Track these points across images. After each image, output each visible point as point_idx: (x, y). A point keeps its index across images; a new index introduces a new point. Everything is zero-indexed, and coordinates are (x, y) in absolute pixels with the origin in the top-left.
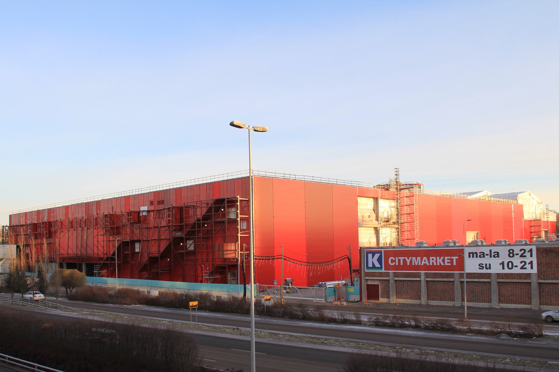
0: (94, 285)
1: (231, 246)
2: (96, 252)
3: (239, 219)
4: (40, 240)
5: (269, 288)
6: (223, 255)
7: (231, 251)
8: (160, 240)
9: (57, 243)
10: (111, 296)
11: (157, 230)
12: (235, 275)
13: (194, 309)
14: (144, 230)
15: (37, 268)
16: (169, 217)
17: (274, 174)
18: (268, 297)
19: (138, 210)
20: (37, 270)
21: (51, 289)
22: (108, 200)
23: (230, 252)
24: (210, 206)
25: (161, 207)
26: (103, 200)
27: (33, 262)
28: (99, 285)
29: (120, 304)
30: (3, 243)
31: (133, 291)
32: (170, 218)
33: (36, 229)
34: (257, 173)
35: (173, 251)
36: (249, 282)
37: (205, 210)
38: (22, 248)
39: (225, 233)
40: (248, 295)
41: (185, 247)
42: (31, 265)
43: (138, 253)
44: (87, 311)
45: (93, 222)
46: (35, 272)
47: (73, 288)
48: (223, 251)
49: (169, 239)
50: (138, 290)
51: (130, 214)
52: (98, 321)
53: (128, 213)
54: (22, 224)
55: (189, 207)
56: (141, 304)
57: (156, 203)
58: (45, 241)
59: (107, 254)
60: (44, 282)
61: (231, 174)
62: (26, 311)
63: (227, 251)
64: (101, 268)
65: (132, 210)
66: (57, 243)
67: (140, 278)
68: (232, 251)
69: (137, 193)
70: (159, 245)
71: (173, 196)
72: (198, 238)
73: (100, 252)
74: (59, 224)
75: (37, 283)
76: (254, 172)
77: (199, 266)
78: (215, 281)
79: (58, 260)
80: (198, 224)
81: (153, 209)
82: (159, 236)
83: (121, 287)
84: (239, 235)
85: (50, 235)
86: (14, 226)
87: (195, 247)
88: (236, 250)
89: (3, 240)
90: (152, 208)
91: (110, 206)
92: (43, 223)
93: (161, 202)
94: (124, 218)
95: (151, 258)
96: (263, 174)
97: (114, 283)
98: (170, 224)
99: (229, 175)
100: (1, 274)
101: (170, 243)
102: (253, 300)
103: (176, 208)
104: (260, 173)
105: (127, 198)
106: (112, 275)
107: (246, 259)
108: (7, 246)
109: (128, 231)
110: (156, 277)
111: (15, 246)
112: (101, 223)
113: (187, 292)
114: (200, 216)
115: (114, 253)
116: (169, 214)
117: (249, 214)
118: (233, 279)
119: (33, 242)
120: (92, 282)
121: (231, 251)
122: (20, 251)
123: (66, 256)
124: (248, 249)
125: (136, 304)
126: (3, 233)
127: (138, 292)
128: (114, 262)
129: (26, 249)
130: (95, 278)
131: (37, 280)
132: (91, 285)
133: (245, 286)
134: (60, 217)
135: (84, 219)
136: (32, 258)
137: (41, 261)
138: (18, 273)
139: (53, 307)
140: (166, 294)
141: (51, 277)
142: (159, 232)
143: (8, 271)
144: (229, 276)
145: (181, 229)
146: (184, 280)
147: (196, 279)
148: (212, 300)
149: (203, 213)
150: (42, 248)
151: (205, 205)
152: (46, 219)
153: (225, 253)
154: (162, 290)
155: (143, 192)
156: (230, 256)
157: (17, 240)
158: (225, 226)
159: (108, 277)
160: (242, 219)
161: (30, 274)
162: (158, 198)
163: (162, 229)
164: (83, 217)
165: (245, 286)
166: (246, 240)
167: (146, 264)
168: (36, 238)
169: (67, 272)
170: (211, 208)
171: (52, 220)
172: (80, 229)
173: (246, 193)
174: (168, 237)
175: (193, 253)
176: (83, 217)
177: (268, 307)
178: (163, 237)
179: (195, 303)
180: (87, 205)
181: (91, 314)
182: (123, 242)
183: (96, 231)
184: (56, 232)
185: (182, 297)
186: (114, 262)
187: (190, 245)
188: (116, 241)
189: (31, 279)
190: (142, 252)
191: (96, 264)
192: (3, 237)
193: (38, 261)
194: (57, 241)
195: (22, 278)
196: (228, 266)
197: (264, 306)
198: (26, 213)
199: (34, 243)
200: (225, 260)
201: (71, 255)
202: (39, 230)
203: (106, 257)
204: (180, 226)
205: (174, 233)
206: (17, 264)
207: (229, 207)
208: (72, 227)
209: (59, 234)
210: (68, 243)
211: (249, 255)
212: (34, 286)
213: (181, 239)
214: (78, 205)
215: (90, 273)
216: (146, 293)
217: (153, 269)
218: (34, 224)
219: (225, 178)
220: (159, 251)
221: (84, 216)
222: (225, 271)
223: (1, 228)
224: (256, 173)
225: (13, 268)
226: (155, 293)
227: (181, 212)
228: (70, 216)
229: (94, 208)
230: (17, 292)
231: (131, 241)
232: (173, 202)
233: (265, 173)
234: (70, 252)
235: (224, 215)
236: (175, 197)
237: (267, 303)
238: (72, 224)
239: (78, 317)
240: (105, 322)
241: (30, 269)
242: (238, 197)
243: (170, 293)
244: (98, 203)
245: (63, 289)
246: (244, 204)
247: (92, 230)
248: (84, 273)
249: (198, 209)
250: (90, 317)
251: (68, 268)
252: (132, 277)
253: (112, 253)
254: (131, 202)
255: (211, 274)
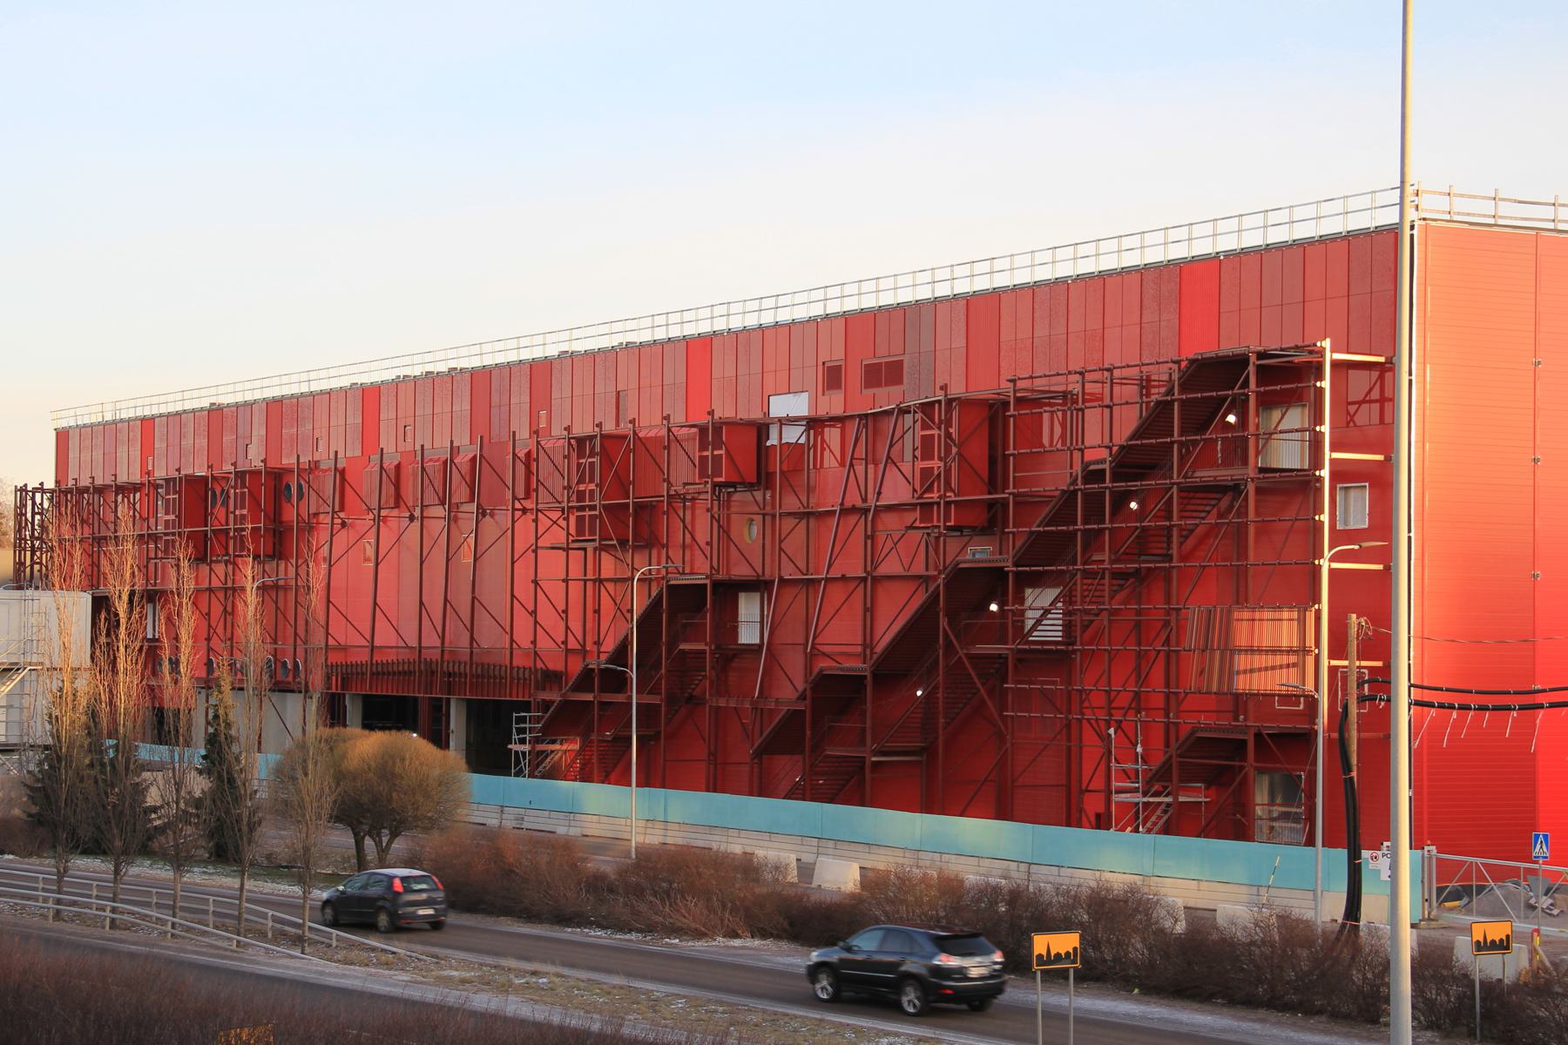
0: (509, 824)
1: (1280, 628)
2: (523, 637)
3: (1325, 473)
4: (220, 569)
5: (1500, 875)
6: (1229, 672)
7: (1275, 651)
8: (872, 581)
9: (318, 584)
10: (598, 885)
11: (858, 528)
12: (1294, 790)
13: (1055, 975)
14: (789, 523)
15: (199, 720)
16: (927, 453)
17: (1549, 212)
18: (1497, 931)
19: (756, 415)
20: (199, 733)
21: (274, 838)
22: (592, 356)
23: (1270, 660)
24: (1157, 394)
25: (885, 398)
26: (570, 358)
27: (180, 690)
28: (534, 821)
29: (650, 929)
30: (20, 579)
31: (719, 862)
32: (936, 464)
33: (201, 512)
34: (1443, 203)
35: (949, 646)
36: (1383, 833)
37: (1127, 422)
38: (122, 608)
39: (1242, 553)
40: (1372, 908)
41: (1011, 626)
42: (168, 704)
43: (754, 650)
44: (468, 965)
45: (515, 476)
46: (188, 744)
47: (394, 835)
48: (1229, 651)
49: (925, 580)
50: (748, 856)
51: (712, 433)
52: (523, 1022)
53: (703, 430)
54: (123, 478)
55: (1036, 402)
56: (763, 934)
57: (854, 376)
58: (249, 575)
59: (583, 652)
60: (237, 800)
61: (1282, 216)
62: (132, 955)
63: (1251, 650)
64: (551, 731)
65: (724, 411)
66: (318, 584)
67: (763, 787)
68: (1281, 653)
69: (751, 321)
70: (870, 611)
71: (952, 339)
72: (1087, 574)
73: (544, 644)
74: (328, 485)
75: (198, 803)
76: (1424, 201)
77: (1089, 736)
78: (1178, 823)
79: (317, 679)
80: (1093, 497)
81: (838, 411)
82: (872, 559)
83: (654, 838)
84: (1325, 565)
85: (279, 542)
86: (81, 491)
87: (1068, 627)
88: (1303, 651)
89: (19, 565)
90: (834, 404)
91: (605, 389)
92: (240, 475)
93: (885, 373)
94: (678, 456)
95: (839, 387)
96: (1480, 210)
97: (620, 816)
98: (934, 496)
99: (1273, 218)
100: (5, 749)
101: (933, 601)
102: (1407, 943)
103: (965, 404)
104: (1461, 205)
105: (699, 349)
106: (605, 766)
107: (1362, 700)
108: (44, 599)
109: (703, 529)
110: (850, 785)
111: (85, 600)
112: (556, 484)
113: (1018, 875)
114: (1105, 454)
115: (623, 647)
116: (927, 442)
117: (1387, 444)
118: (1285, 816)
119: (183, 577)
120: (499, 804)
121: (1275, 651)
122: (114, 625)
123: (364, 657)
124: (1379, 645)
125: (736, 936)
126: (19, 529)
127: (748, 868)
128: (620, 698)
129: (143, 617)
130: (512, 780)
131: (199, 785)
132: (493, 822)
133: (1354, 856)
134: (336, 443)
135: (462, 460)
136: (175, 664)
137: (226, 687)
138: (96, 748)
139: (280, 937)
140: (904, 881)
141: (279, 771)
142: (871, 537)
143: (41, 732)
144: (1261, 796)
145: (991, 521)
146: (1003, 812)
147: (1073, 807)
148: (1162, 931)
149: (1122, 435)
150: (230, 613)
151: (1131, 392)
152: (255, 458)
153: (1241, 661)
154: (881, 862)
155: (784, 316)
156: (1261, 678)
157: (95, 565)
158: (1243, 512)
159: (586, 777)
160: (1342, 474)
161: (161, 752)
162: (868, 350)
163: (891, 522)
164: (454, 451)
165: (1354, 856)
166: (1371, 596)
167: (794, 717)
168: (201, 558)
169: (366, 745)
170: (1164, 407)
171: (288, 461)
172: (439, 511)
173: (1379, 320)
174: (919, 569)
175: (1055, 659)
176: (454, 451)
177: (1492, 989)
178: (890, 566)
179: (1065, 942)
180: (482, 381)
181: (486, 983)
182: (671, 588)
183: (525, 525)
184: (309, 527)
185: (993, 903)
186: (620, 698)
187: (1042, 614)
188: (635, 582)
189: (168, 780)
190: (770, 649)
191: (526, 706)
192: (19, 545)
193: (208, 684)
194: (317, 575)
195: (117, 772)
196: (1258, 736)
197: (1465, 978)
198: (147, 423)
199: (189, 586)
200: (1241, 702)
201: (391, 657)
202: (219, 511)
203: (576, 667)
204: (991, 504)
205: (953, 545)
206: (98, 700)
207: (1268, 402)
208: (398, 500)
209: (324, 535)
210: (378, 588)
211: (1382, 681)
212: (184, 817)
213: (992, 581)
214: (431, 379)
215: (490, 757)
216: (793, 876)
217: (835, 741)
218: (193, 482)
219: (1253, 240)
220: (868, 645)
221: (462, 440)
222: (1233, 770)
223: (10, 500)
224: (1433, 206)
225: (73, 719)
226: (840, 876)
227: (993, 427)
228: (388, 443)
229: (521, 399)
230: (86, 852)
231: (717, 585)
232: (949, 373)
233: (1488, 208)
234: (385, 637)
235: (1238, 449)
236: (960, 342)
237: (1491, 967)
238: (397, 485)
239: (415, 993)
240: (561, 1028)
241: (162, 726)
242: (1327, 344)
243: (925, 879)
244: (540, 373)
245: (341, 839)
246: (1359, 384)
247: (504, 518)
248: (455, 755)
249: (1093, 417)
250: (483, 1001)
251: (369, 724)
252: (716, 784)
253: (609, 645)
254: (723, 367)
255: (1160, 779)
